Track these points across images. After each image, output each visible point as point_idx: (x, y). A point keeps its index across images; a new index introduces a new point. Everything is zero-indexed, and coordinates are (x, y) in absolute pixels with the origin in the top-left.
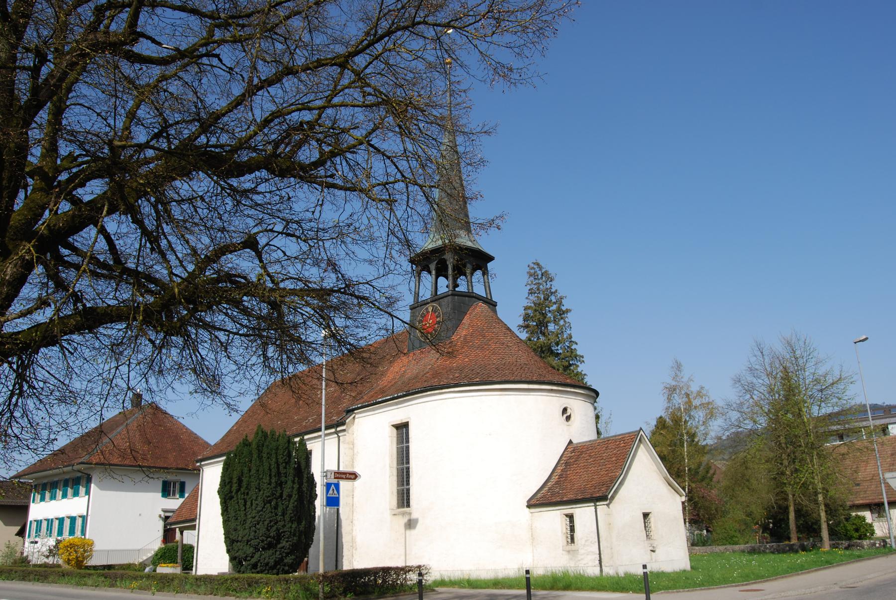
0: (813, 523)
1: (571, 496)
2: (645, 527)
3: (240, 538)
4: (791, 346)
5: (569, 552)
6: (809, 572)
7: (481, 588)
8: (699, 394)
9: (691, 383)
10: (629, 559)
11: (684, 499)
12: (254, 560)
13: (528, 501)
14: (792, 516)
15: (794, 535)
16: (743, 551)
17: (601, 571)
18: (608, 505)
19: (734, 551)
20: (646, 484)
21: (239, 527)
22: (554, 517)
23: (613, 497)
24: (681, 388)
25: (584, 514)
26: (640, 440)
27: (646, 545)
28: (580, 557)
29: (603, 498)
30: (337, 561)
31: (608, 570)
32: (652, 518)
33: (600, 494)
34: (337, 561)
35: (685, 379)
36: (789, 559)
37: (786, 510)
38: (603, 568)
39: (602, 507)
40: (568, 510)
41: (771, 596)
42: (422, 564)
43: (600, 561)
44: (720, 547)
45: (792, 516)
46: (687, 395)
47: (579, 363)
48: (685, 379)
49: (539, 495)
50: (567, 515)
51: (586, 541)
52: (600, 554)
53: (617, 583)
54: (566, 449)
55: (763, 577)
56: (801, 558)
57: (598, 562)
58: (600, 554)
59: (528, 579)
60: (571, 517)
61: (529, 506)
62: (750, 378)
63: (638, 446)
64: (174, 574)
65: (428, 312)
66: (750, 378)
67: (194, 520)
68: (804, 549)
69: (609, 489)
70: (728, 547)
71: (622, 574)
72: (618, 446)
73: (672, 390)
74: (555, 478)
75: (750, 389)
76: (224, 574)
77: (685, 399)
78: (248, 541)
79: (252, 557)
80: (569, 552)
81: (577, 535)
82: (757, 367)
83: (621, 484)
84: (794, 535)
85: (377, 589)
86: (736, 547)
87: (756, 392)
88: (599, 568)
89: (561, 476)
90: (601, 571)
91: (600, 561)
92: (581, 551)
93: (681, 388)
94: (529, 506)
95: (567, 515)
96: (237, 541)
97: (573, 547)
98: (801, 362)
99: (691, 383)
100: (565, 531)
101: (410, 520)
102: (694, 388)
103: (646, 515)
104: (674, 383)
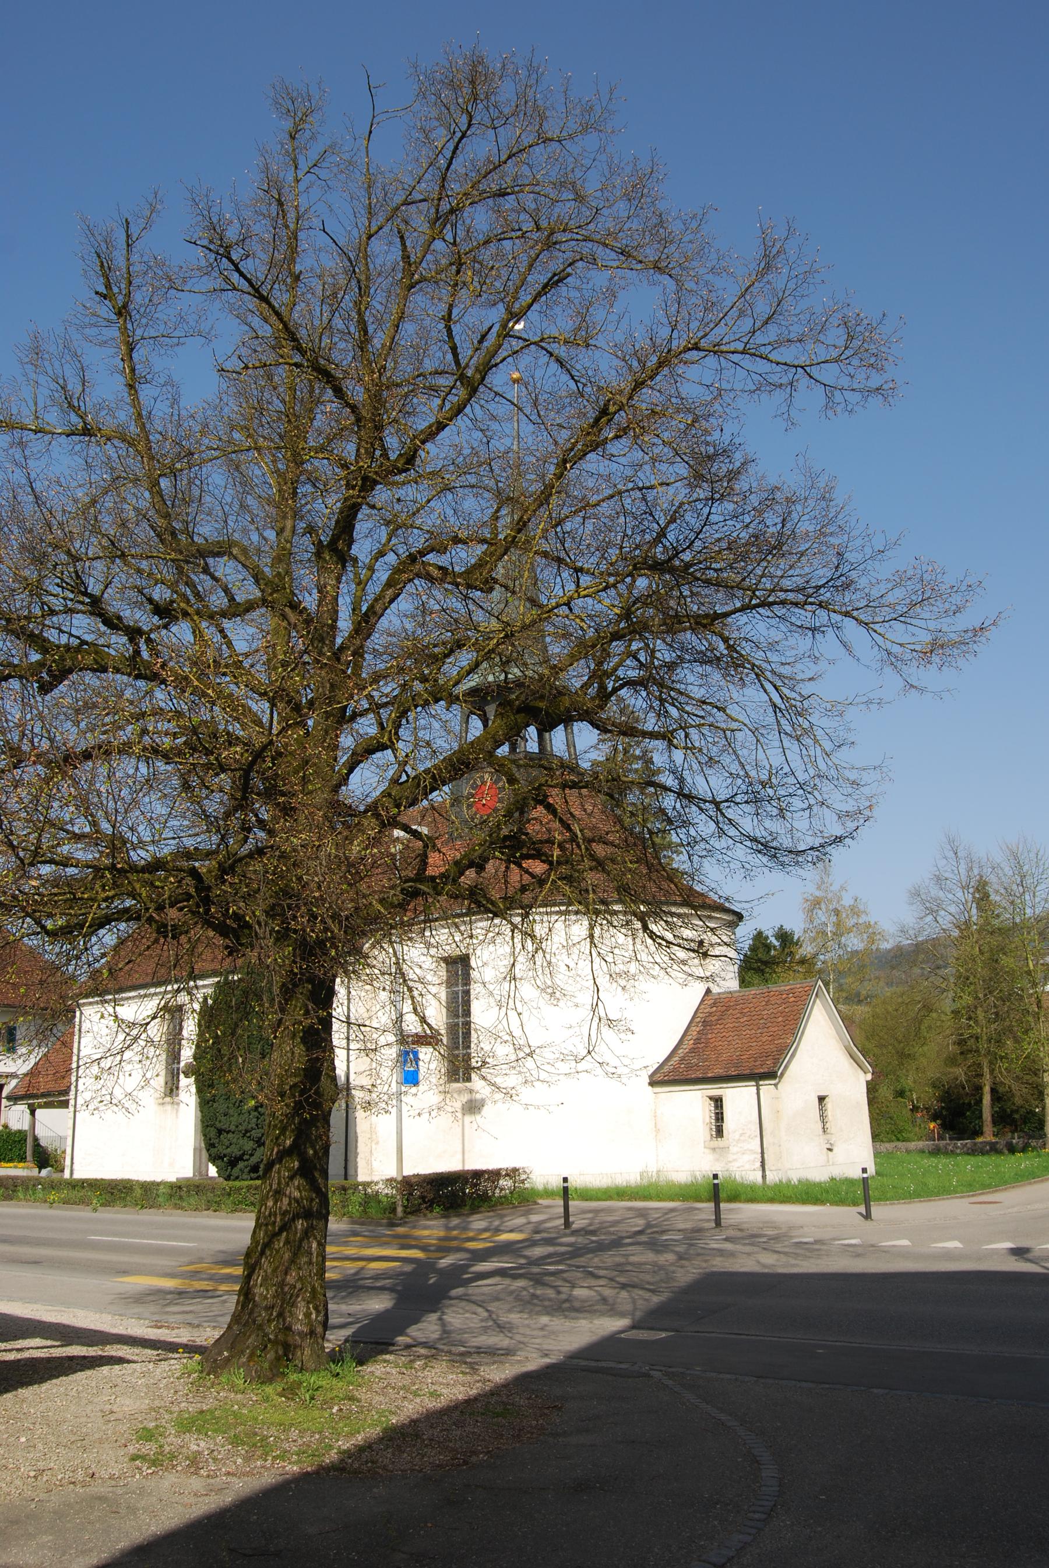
0: (1012, 1111)
1: (719, 1071)
2: (822, 1116)
3: (233, 1128)
4: (1016, 857)
5: (714, 1149)
6: (1042, 1181)
7: (599, 1200)
8: (855, 911)
9: (843, 893)
10: (803, 1160)
11: (869, 1077)
12: (254, 1160)
13: (651, 1076)
14: (987, 1099)
15: (988, 1128)
16: (922, 1151)
17: (764, 1177)
18: (776, 1085)
19: (908, 1151)
20: (824, 1060)
21: (231, 1111)
22: (693, 1102)
23: (782, 1074)
24: (830, 901)
25: (739, 1098)
26: (817, 995)
27: (821, 1142)
28: (731, 1157)
29: (771, 1075)
30: (346, 1160)
31: (772, 1177)
32: (829, 1104)
33: (764, 1069)
34: (346, 1160)
35: (835, 887)
36: (969, 1164)
37: (979, 1089)
38: (767, 1173)
39: (767, 1088)
40: (714, 1090)
41: (1015, 1209)
42: (517, 1166)
43: (763, 1163)
44: (887, 1145)
45: (987, 1099)
46: (837, 912)
47: (674, 856)
48: (835, 887)
49: (666, 1069)
50: (711, 1098)
51: (741, 1135)
52: (762, 1153)
53: (807, 1193)
54: (703, 1001)
55: (989, 1186)
56: (1022, 1161)
57: (758, 1164)
58: (762, 1153)
59: (566, 1190)
60: (718, 1102)
61: (652, 1084)
62: (935, 892)
63: (814, 1002)
64: (27, 1177)
65: (484, 783)
66: (935, 892)
67: (66, 1092)
68: (1012, 1150)
69: (777, 1062)
70: (900, 1144)
71: (795, 1181)
72: (785, 1001)
73: (816, 903)
74: (689, 1044)
75: (933, 910)
76: (188, 1179)
77: (834, 919)
78: (247, 1131)
79: (252, 1155)
80: (714, 1149)
81: (728, 1125)
82: (946, 875)
83: (793, 1056)
84: (988, 1128)
85: (469, 1202)
86: (912, 1145)
87: (942, 913)
88: (760, 1173)
89: (697, 1041)
90: (764, 1177)
91: (763, 1163)
92: (733, 1149)
93: (830, 901)
94: (652, 1084)
95: (711, 1098)
96: (228, 1132)
97: (720, 1143)
98: (1029, 881)
99: (843, 893)
100: (708, 1120)
101: (471, 1101)
102: (847, 901)
103: (821, 1099)
104: (818, 893)
